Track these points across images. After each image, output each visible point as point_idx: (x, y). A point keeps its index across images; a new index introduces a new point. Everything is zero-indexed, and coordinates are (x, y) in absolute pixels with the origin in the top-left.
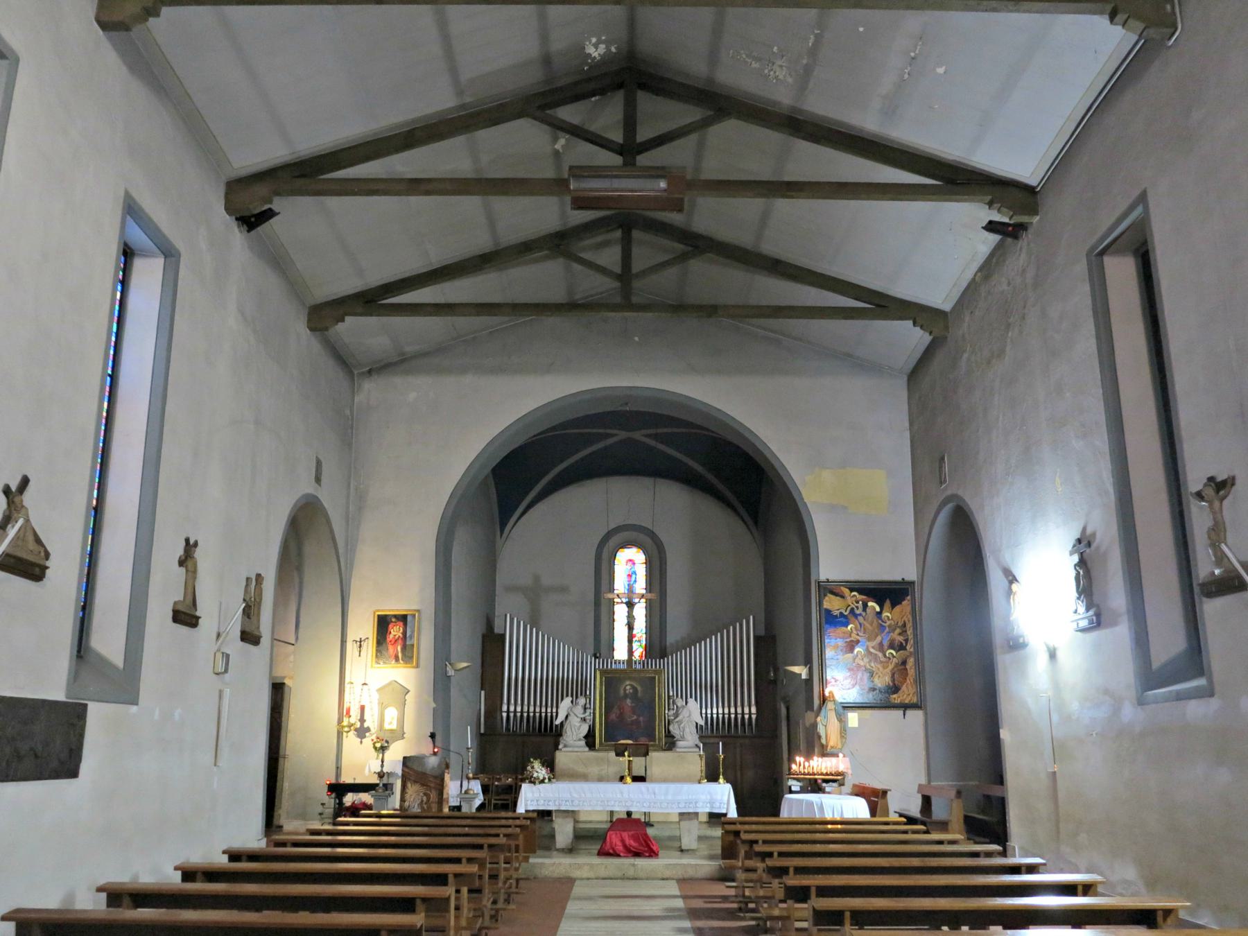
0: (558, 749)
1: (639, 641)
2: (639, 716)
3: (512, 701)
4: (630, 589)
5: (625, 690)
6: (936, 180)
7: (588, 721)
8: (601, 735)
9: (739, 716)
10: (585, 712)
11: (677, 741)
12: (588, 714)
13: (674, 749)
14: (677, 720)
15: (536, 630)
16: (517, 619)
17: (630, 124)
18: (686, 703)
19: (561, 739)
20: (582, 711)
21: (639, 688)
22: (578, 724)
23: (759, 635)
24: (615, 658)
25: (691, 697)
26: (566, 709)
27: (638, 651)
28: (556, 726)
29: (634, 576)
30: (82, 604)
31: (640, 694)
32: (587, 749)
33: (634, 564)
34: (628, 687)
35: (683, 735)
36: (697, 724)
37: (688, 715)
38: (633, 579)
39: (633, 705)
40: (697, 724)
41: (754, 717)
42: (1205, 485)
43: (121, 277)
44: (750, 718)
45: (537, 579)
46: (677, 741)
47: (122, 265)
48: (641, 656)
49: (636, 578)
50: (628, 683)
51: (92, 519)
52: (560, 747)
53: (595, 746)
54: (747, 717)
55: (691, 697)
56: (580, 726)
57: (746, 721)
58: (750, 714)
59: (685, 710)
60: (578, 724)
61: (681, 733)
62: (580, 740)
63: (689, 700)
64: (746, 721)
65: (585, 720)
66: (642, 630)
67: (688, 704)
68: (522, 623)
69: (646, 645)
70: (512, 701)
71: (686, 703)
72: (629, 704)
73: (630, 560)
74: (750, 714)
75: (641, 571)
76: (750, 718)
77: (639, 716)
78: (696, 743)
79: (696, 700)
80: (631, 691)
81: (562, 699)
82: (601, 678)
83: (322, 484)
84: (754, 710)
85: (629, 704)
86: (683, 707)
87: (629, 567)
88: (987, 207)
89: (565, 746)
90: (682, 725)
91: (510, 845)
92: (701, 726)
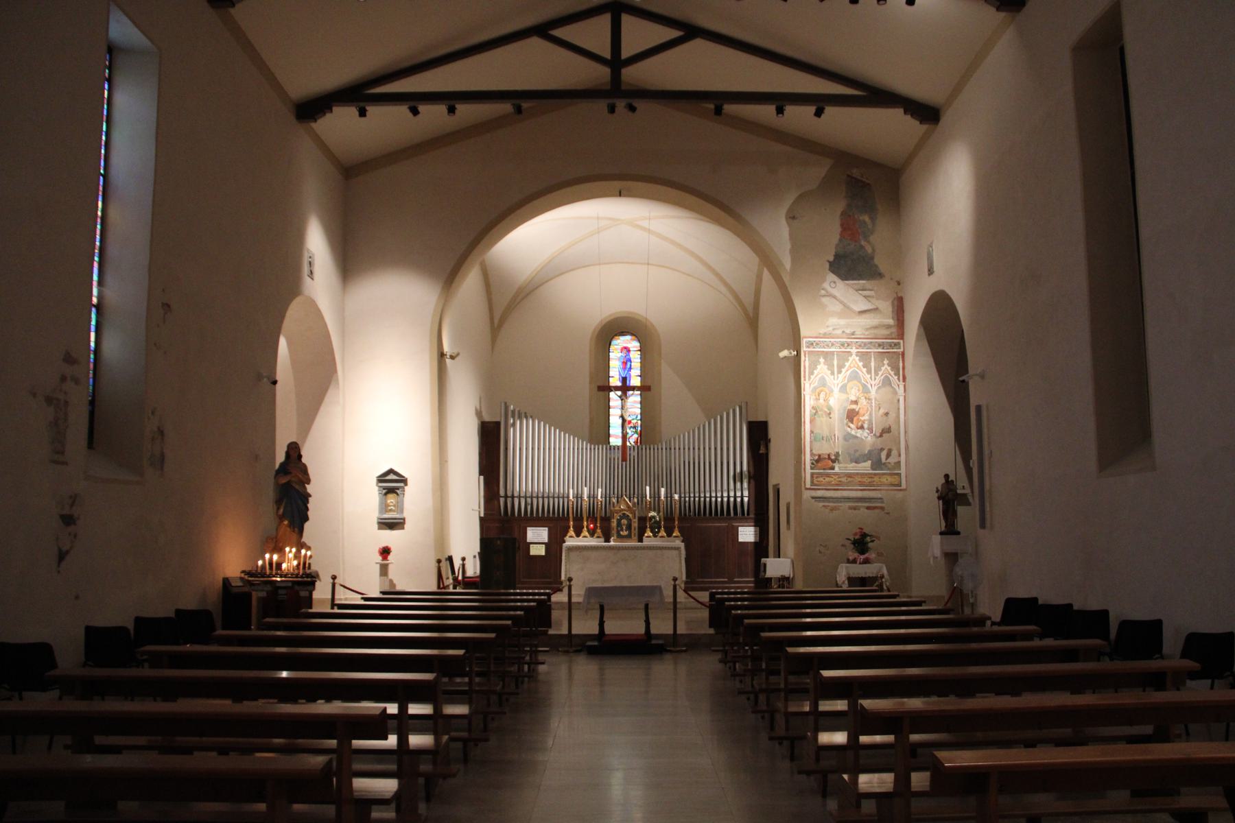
1: (635, 427)
4: (623, 398)
6: (856, 89)
9: (732, 499)
15: (764, 631)
17: (617, 388)
23: (751, 420)
24: (611, 444)
27: (633, 438)
29: (629, 364)
30: (90, 398)
33: (629, 351)
38: (628, 366)
41: (746, 499)
42: (391, 581)
43: (107, 75)
45: (363, 113)
47: (107, 63)
48: (636, 442)
49: (631, 365)
51: (935, 607)
54: (739, 500)
66: (637, 417)
69: (641, 431)
73: (625, 348)
75: (636, 357)
83: (315, 278)
87: (623, 355)
91: (578, 534)
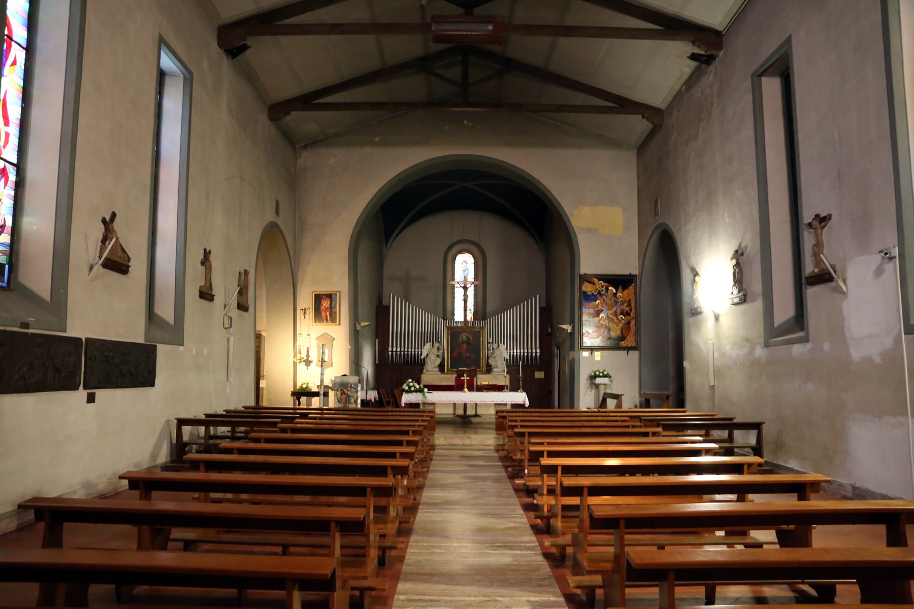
5: (462, 338)
21: (471, 338)
32: (440, 373)
34: (464, 337)
39: (467, 347)
41: (538, 354)
44: (536, 355)
50: (464, 334)
52: (424, 371)
55: (501, 343)
58: (536, 353)
62: (436, 368)
68: (400, 299)
70: (395, 345)
74: (536, 353)
80: (466, 339)
84: (538, 351)
89: (427, 371)
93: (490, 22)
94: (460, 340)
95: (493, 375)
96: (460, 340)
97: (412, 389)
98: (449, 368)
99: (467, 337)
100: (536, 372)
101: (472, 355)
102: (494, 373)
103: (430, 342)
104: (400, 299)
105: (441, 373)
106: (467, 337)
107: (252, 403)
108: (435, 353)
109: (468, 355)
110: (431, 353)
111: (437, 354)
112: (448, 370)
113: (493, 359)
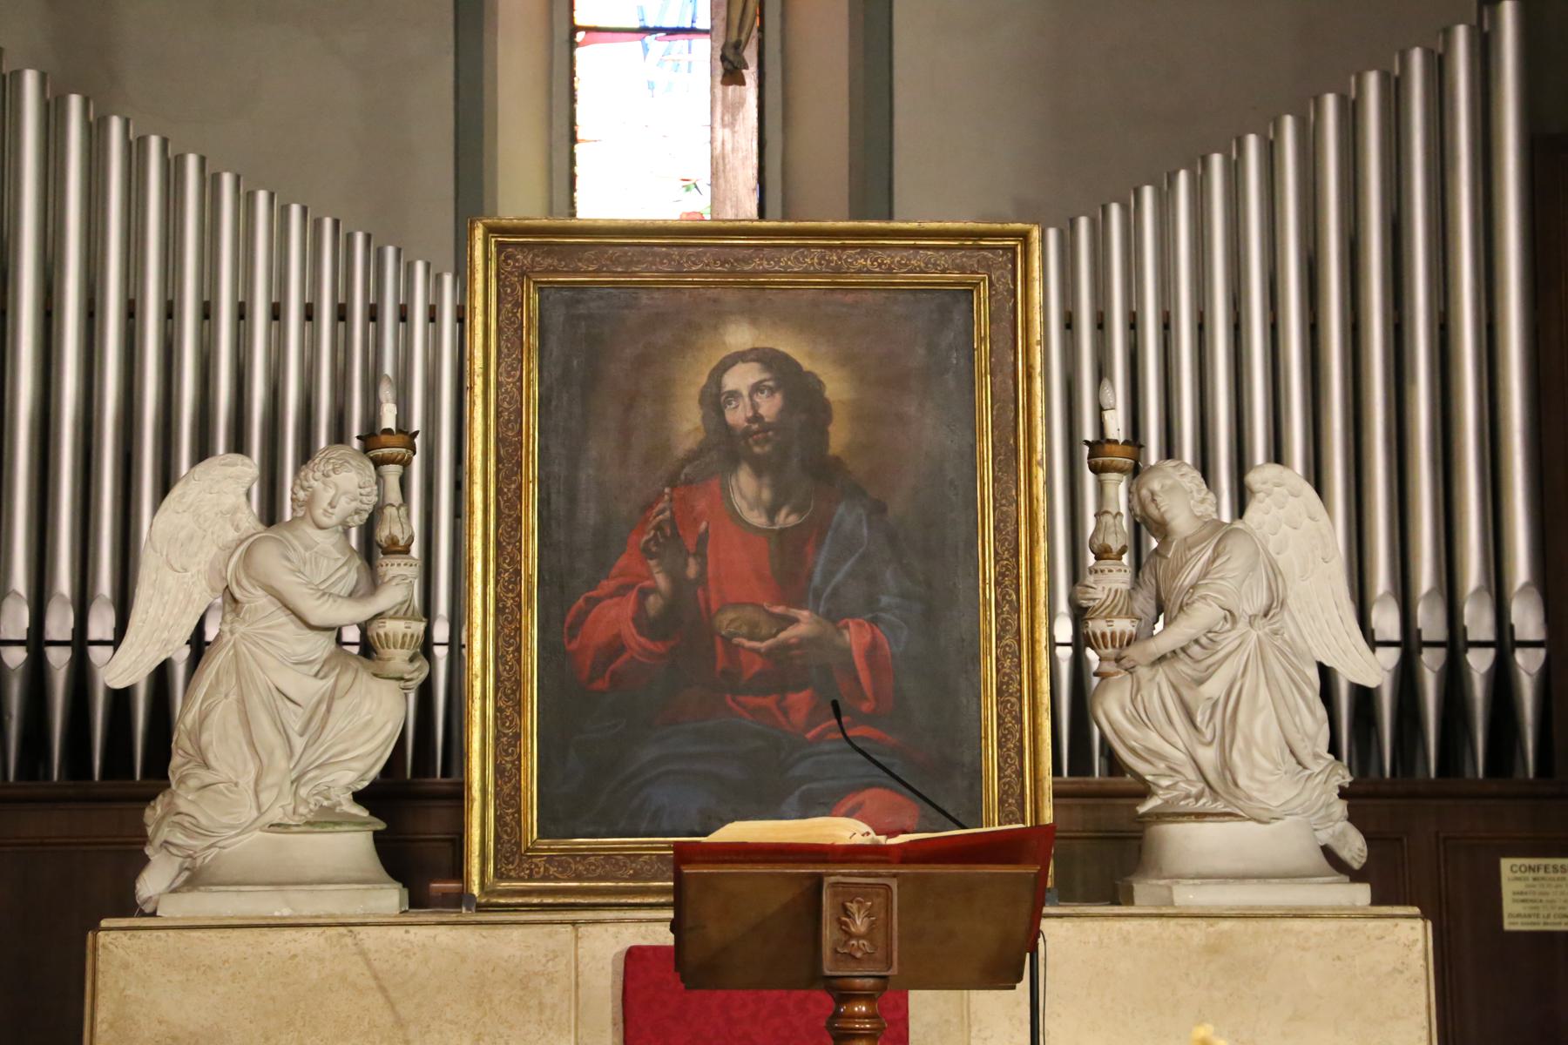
0: (126, 905)
2: (835, 616)
3: (64, 580)
5: (715, 399)
7: (398, 659)
8: (507, 774)
10: (373, 582)
11: (1159, 816)
12: (388, 598)
13: (1144, 890)
14: (1166, 637)
16: (202, 162)
18: (1241, 504)
19: (154, 813)
20: (352, 574)
21: (836, 387)
22: (307, 687)
25: (1277, 454)
26: (206, 554)
28: (121, 699)
31: (839, 437)
32: (391, 897)
34: (740, 379)
35: (1226, 765)
36: (1326, 673)
37: (1261, 600)
39: (785, 519)
40: (1326, 673)
41: (1528, 664)
44: (1502, 675)
46: (1159, 816)
50: (740, 336)
52: (151, 884)
53: (457, 870)
55: (1277, 454)
56: (331, 698)
57: (1479, 689)
58: (1504, 642)
59: (1236, 558)
60: (307, 687)
61: (1208, 756)
62: (326, 819)
63: (1262, 474)
64: (1479, 689)
65: (367, 648)
67: (1250, 513)
68: (227, 180)
70: (64, 580)
71: (1241, 504)
72: (757, 519)
74: (1504, 642)
76: (1502, 675)
77: (835, 616)
78: (1324, 837)
79: (1317, 476)
80: (769, 406)
81: (165, 483)
82: (508, 298)
84: (1527, 620)
85: (757, 519)
86: (1218, 534)
88: (1142, 449)
89: (194, 879)
90: (1214, 687)
92: (1364, 697)
93: (836, 1027)
94: (689, 423)
95: (1168, 914)
96: (689, 423)
97: (552, 877)
98: (532, 817)
99: (769, 359)
100: (1506, 864)
101: (854, 637)
102: (1188, 896)
103: (238, 444)
104: (227, 180)
105: (418, 900)
106: (769, 359)
107: (1471, 637)
108: (323, 612)
109: (805, 624)
110: (254, 599)
111: (349, 615)
112: (509, 852)
113: (1158, 688)
